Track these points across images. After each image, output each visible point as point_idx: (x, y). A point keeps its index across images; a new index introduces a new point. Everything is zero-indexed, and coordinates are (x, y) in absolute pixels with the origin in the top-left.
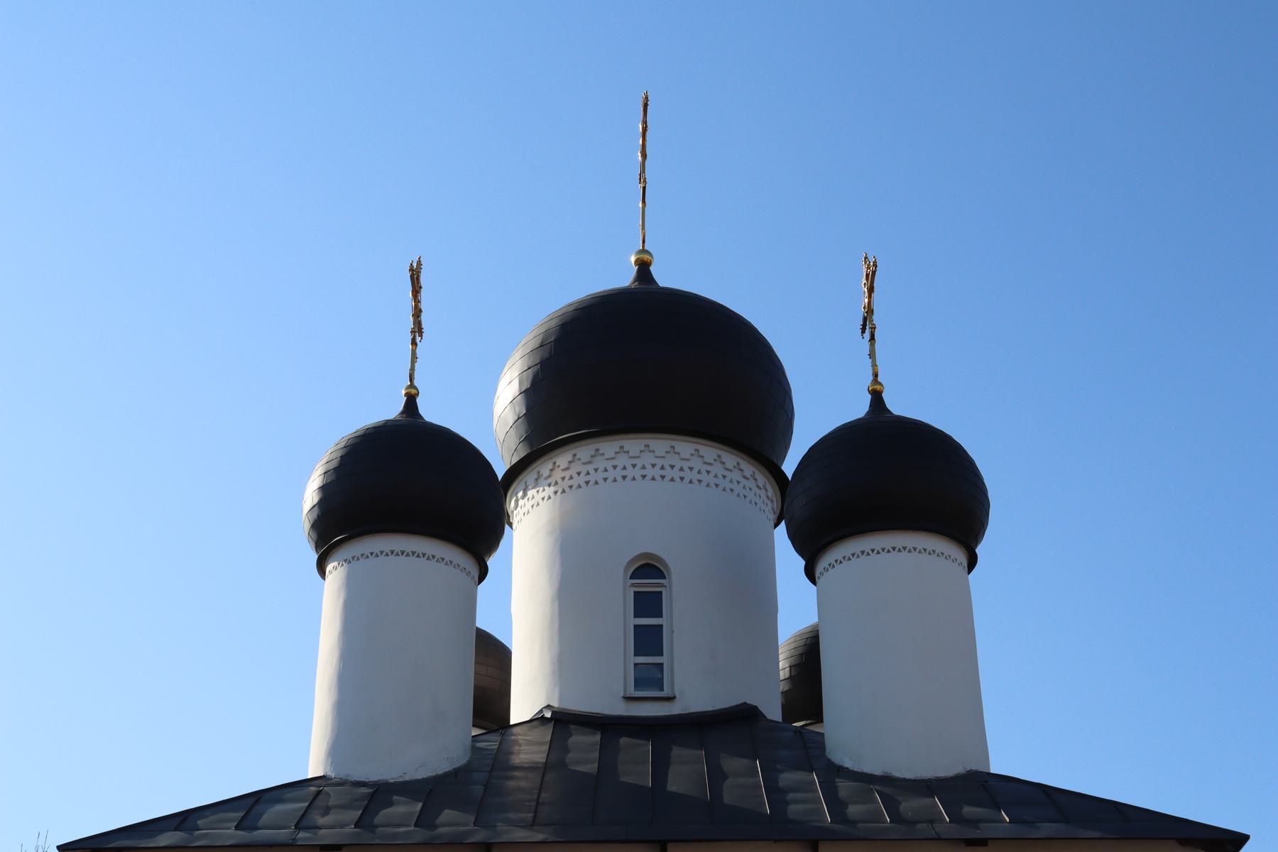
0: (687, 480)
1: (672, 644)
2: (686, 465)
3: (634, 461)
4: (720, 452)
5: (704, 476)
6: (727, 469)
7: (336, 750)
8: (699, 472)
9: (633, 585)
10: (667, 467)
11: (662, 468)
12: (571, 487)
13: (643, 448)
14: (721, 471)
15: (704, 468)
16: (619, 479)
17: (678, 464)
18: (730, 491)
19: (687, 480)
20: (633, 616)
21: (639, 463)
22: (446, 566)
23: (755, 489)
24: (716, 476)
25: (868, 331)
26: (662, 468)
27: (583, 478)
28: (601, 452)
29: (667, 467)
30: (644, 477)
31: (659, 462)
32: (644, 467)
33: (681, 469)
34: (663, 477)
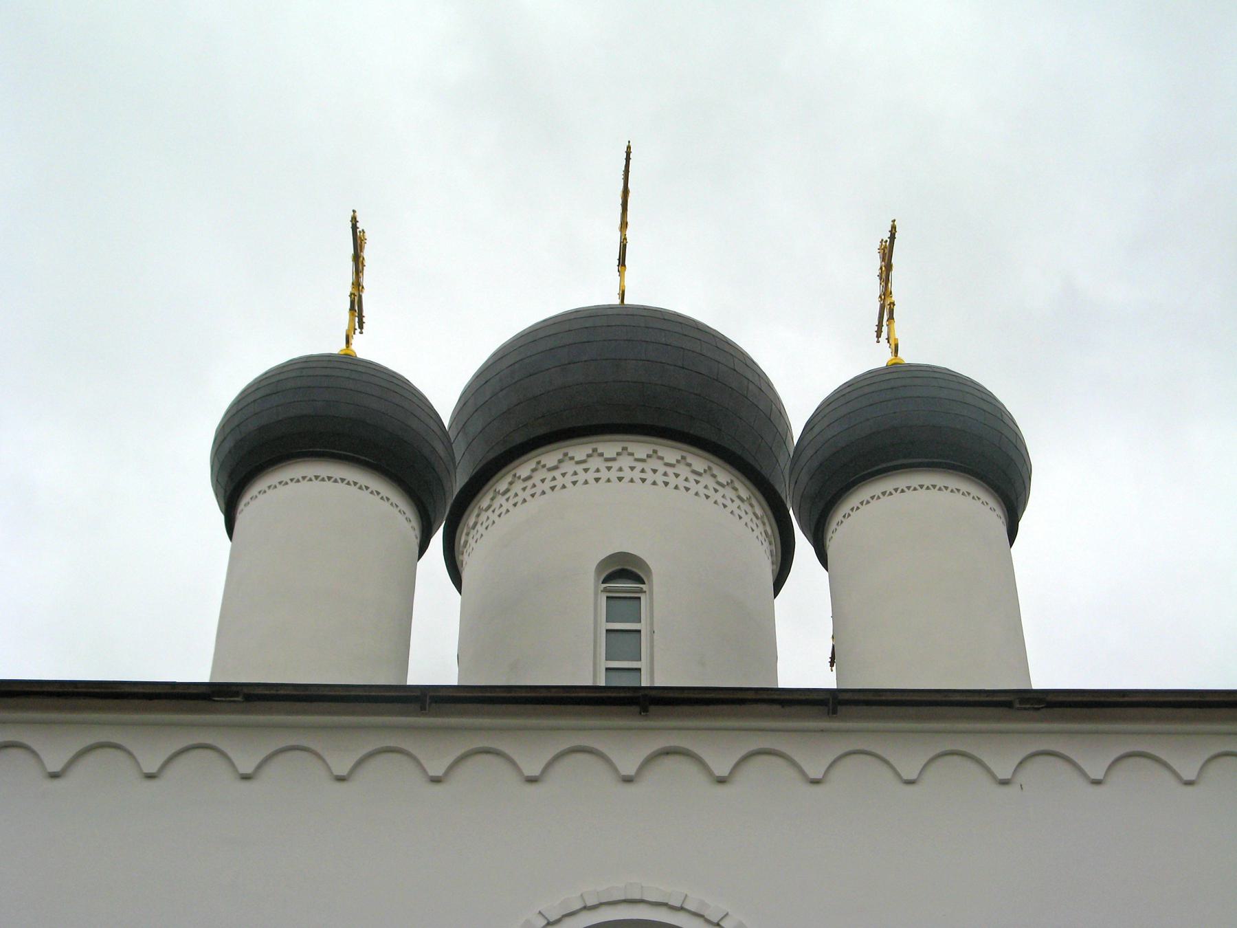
0: (671, 485)
1: (652, 647)
2: (670, 471)
4: (711, 465)
5: (691, 484)
6: (607, 460)
7: (213, 673)
8: (686, 480)
9: (605, 590)
10: (648, 470)
11: (643, 471)
12: (515, 505)
13: (620, 450)
14: (711, 484)
15: (692, 477)
17: (662, 469)
18: (722, 506)
19: (671, 485)
20: (604, 658)
21: (615, 465)
22: (371, 495)
23: (738, 502)
24: (706, 487)
25: (884, 335)
26: (643, 471)
27: (548, 484)
28: (542, 463)
29: (648, 470)
30: (620, 479)
31: (639, 466)
32: (620, 469)
33: (665, 474)
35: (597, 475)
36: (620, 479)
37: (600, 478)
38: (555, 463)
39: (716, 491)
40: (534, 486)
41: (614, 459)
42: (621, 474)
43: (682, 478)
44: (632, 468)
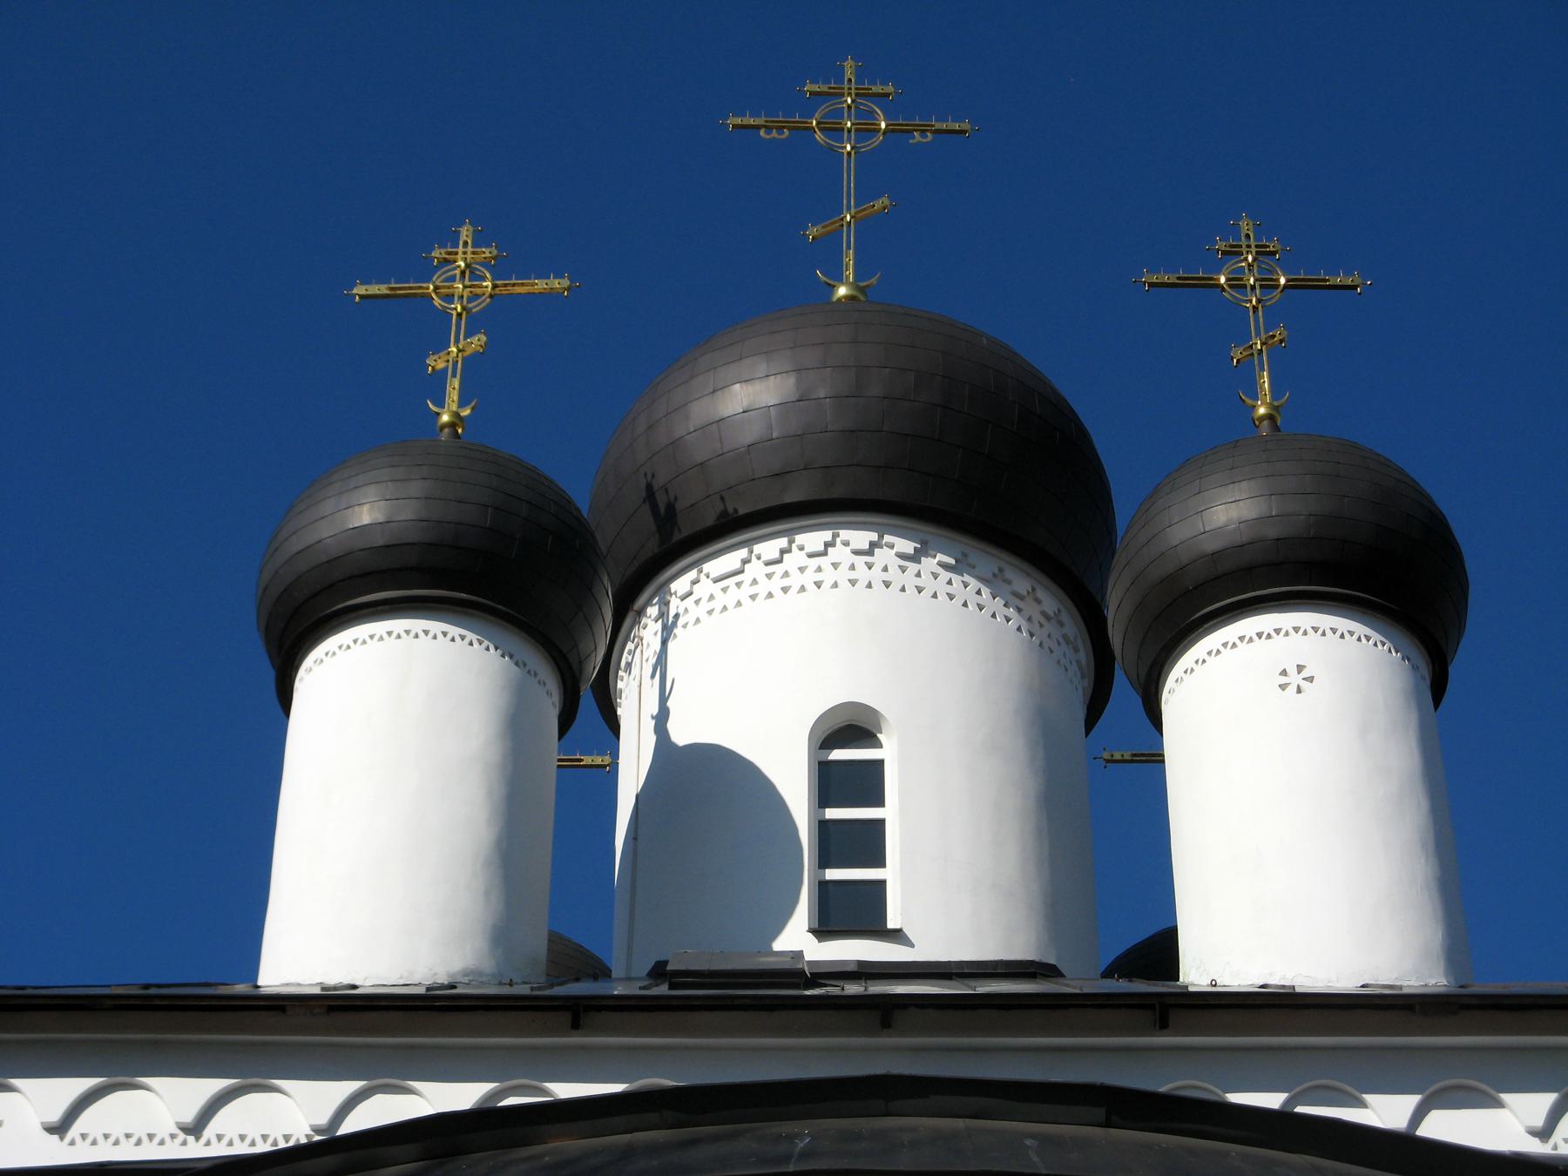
3: (771, 569)
11: (819, 569)
12: (710, 612)
16: (777, 592)
30: (853, 582)
34: (818, 584)
35: (818, 577)
36: (785, 590)
37: (757, 595)
38: (687, 588)
39: (903, 569)
40: (786, 574)
41: (690, 594)
42: (786, 582)
43: (844, 567)
44: (802, 569)
